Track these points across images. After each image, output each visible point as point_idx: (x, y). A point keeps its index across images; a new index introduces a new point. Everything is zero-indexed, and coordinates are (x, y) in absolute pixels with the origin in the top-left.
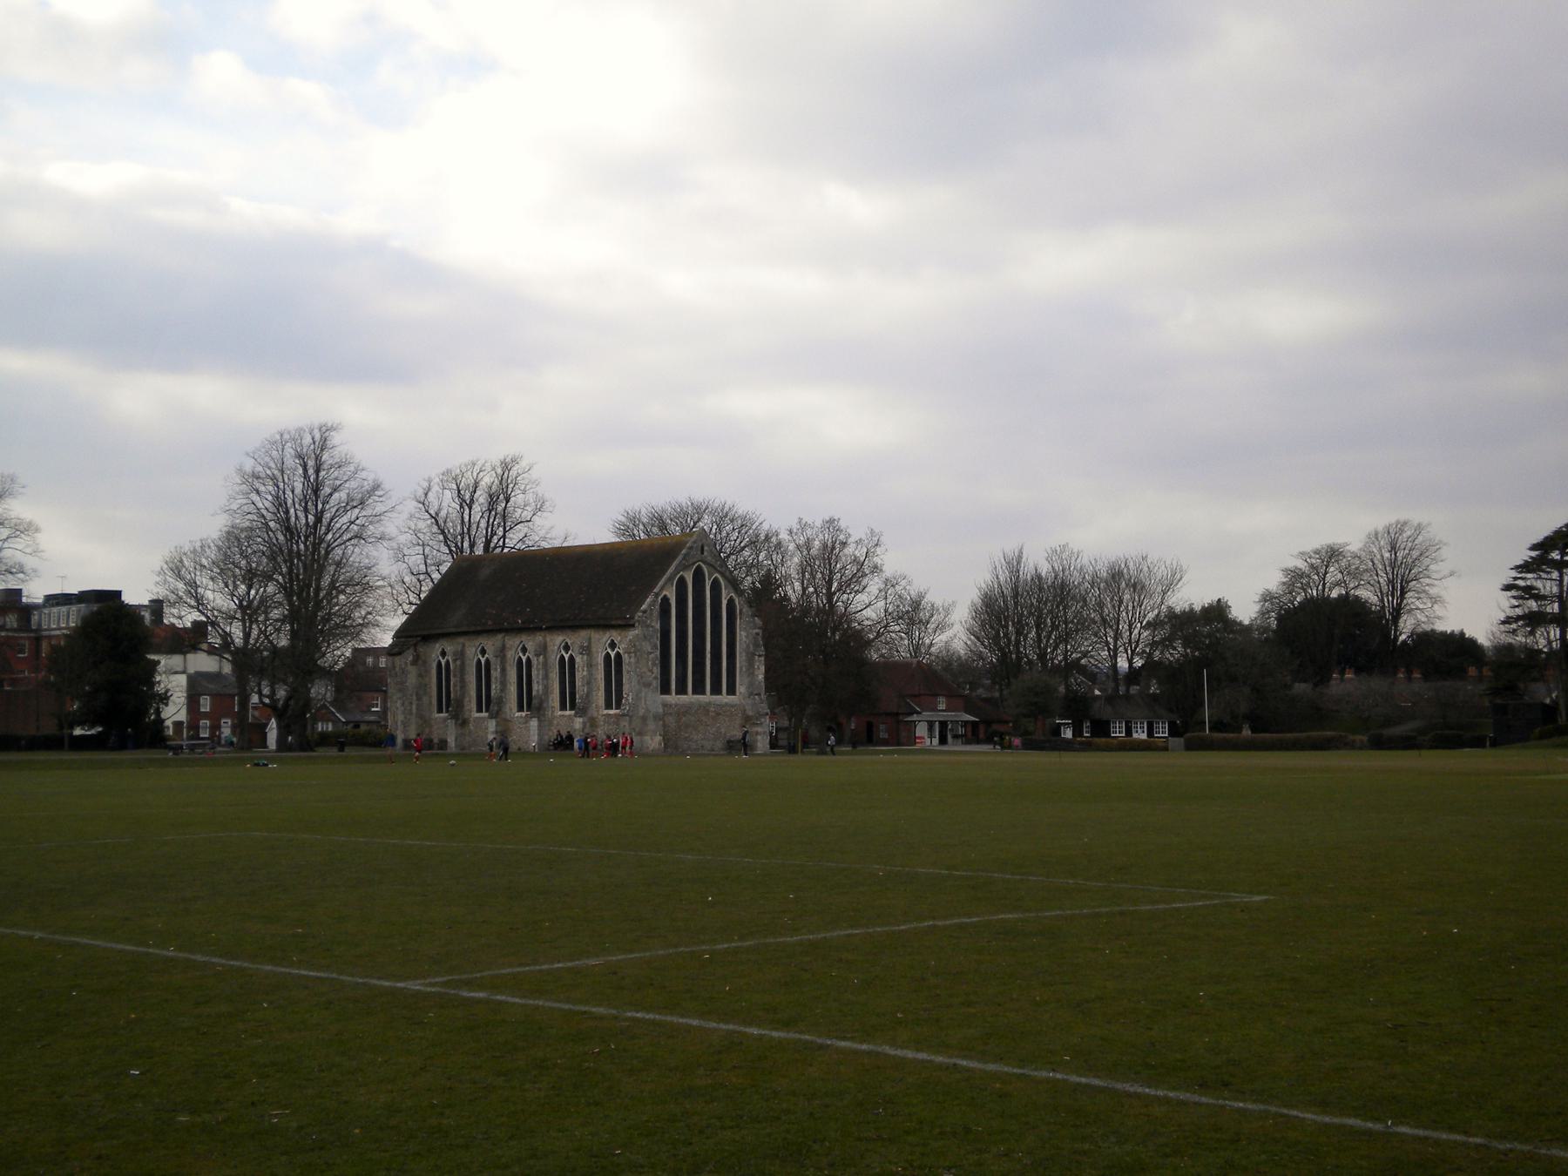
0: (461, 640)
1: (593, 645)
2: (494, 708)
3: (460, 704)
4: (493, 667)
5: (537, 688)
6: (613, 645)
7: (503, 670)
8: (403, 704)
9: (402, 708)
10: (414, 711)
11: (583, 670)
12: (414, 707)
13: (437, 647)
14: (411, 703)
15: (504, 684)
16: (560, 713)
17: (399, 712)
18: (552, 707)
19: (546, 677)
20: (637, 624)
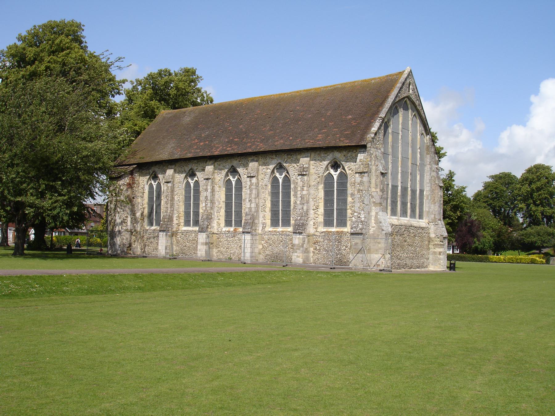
11: (303, 190)
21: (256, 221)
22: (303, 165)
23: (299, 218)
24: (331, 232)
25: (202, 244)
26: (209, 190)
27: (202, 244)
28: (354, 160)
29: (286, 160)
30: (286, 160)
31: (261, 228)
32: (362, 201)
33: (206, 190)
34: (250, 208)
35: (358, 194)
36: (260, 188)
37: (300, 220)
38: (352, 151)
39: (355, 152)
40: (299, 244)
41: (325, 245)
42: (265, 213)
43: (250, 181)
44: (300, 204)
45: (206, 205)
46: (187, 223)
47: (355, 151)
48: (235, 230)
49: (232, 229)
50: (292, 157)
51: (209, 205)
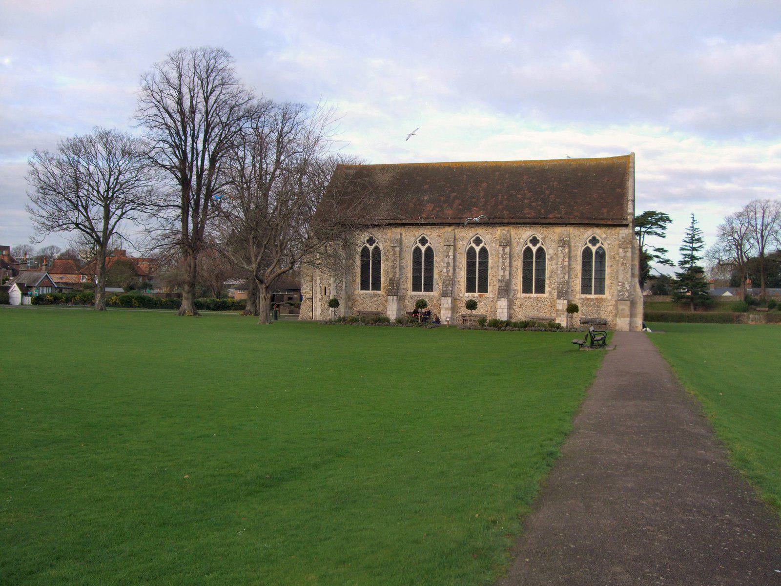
0: (398, 230)
6: (423, 241)
8: (335, 282)
10: (344, 288)
11: (564, 261)
12: (344, 283)
13: (363, 238)
14: (341, 281)
16: (524, 295)
17: (331, 288)
23: (561, 286)
25: (446, 309)
27: (446, 309)
29: (541, 232)
30: (541, 232)
34: (503, 276)
37: (562, 287)
44: (562, 273)
45: (447, 272)
46: (364, 286)
47: (614, 229)
48: (479, 295)
51: (451, 271)
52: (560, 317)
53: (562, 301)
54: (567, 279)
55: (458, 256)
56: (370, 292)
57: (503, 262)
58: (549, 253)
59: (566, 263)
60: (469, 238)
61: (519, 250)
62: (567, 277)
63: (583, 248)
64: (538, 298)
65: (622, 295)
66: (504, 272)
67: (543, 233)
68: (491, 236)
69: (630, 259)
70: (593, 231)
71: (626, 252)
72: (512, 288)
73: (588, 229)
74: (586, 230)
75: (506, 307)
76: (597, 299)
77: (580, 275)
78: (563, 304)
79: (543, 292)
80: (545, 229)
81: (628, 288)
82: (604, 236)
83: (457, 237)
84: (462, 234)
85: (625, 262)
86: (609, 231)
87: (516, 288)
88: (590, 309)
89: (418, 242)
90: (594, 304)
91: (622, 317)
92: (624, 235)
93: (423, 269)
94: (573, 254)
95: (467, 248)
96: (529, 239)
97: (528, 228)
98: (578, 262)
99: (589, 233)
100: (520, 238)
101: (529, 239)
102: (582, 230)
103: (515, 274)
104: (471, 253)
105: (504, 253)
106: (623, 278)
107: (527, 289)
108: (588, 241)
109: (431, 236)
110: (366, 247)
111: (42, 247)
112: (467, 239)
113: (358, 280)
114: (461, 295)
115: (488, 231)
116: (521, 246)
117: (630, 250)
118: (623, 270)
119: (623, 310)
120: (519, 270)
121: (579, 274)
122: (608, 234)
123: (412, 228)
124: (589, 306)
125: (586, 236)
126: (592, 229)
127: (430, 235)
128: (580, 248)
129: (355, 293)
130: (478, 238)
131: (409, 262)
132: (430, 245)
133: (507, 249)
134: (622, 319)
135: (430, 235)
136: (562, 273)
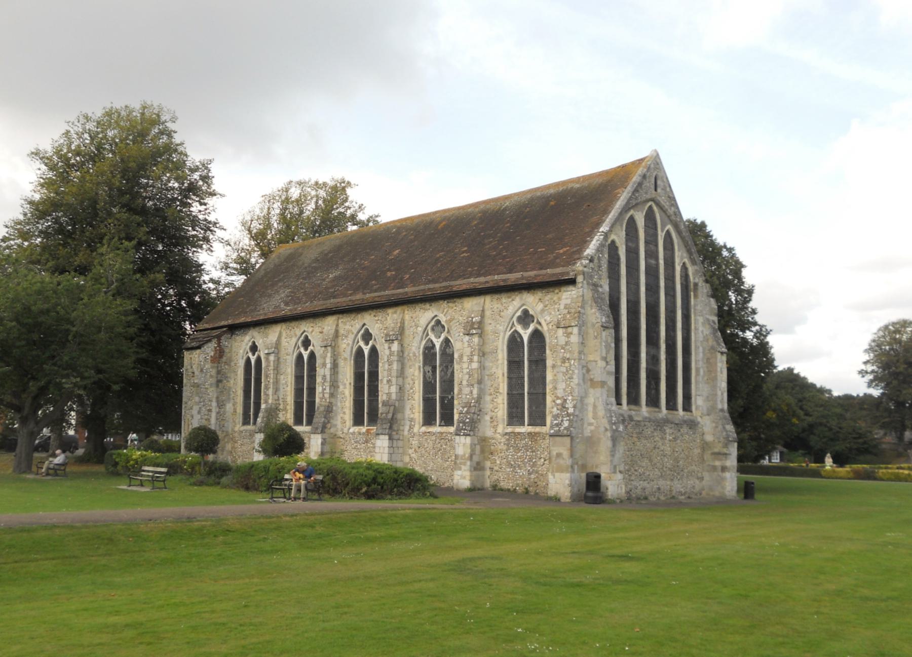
1: (487, 321)
2: (318, 419)
3: (397, 409)
4: (319, 362)
5: (386, 390)
7: (335, 366)
8: (199, 412)
9: (199, 417)
11: (471, 361)
12: (213, 415)
14: (210, 411)
15: (334, 385)
16: (424, 429)
18: (411, 420)
19: (401, 373)
20: (580, 279)
21: (399, 416)
22: (473, 318)
23: (465, 409)
24: (519, 433)
26: (329, 366)
28: (556, 306)
29: (445, 310)
30: (445, 310)
31: (407, 428)
32: (569, 378)
33: (324, 365)
34: (389, 394)
35: (561, 366)
36: (406, 361)
37: (467, 412)
38: (553, 291)
39: (557, 293)
40: (464, 455)
41: (510, 457)
42: (414, 402)
43: (390, 348)
44: (468, 385)
47: (557, 291)
48: (368, 430)
49: (363, 429)
50: (456, 306)
52: (460, 469)
53: (463, 438)
54: (475, 396)
55: (341, 363)
56: (436, 429)
57: (390, 370)
58: (554, 339)
59: (475, 365)
60: (355, 332)
61: (416, 348)
62: (475, 392)
63: (508, 333)
64: (442, 433)
65: (557, 425)
66: (389, 387)
67: (448, 311)
68: (381, 325)
69: (576, 348)
70: (521, 299)
71: (569, 335)
72: (407, 416)
73: (513, 297)
74: (510, 300)
75: (386, 450)
76: (531, 433)
77: (504, 388)
78: (464, 444)
79: (452, 424)
80: (450, 305)
81: (571, 410)
82: (540, 306)
83: (341, 332)
84: (348, 327)
85: (568, 356)
86: (549, 296)
87: (412, 416)
88: (519, 454)
89: (430, 333)
90: (526, 445)
91: (557, 472)
92: (569, 301)
93: (526, 394)
94: (488, 348)
95: (354, 350)
96: (430, 326)
97: (427, 306)
98: (500, 362)
99: (514, 304)
100: (417, 326)
101: (430, 326)
102: (504, 298)
103: (412, 391)
104: (514, 342)
105: (391, 354)
106: (564, 390)
107: (429, 419)
108: (515, 319)
109: (313, 333)
110: (516, 331)
111: (882, 324)
112: (353, 333)
113: (240, 409)
114: (345, 430)
115: (377, 318)
116: (418, 338)
117: (575, 330)
118: (563, 372)
119: (559, 455)
120: (416, 385)
121: (501, 385)
122: (547, 303)
123: (293, 324)
124: (517, 449)
125: (511, 309)
126: (520, 296)
127: (312, 332)
128: (502, 334)
129: (236, 429)
130: (526, 312)
131: (289, 377)
132: (447, 335)
133: (395, 347)
134: (557, 475)
135: (312, 332)
136: (468, 385)
